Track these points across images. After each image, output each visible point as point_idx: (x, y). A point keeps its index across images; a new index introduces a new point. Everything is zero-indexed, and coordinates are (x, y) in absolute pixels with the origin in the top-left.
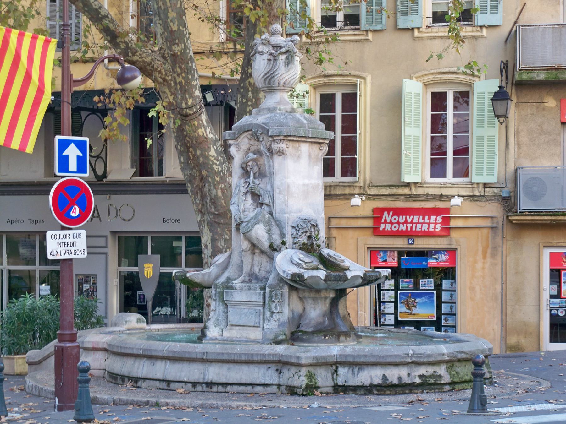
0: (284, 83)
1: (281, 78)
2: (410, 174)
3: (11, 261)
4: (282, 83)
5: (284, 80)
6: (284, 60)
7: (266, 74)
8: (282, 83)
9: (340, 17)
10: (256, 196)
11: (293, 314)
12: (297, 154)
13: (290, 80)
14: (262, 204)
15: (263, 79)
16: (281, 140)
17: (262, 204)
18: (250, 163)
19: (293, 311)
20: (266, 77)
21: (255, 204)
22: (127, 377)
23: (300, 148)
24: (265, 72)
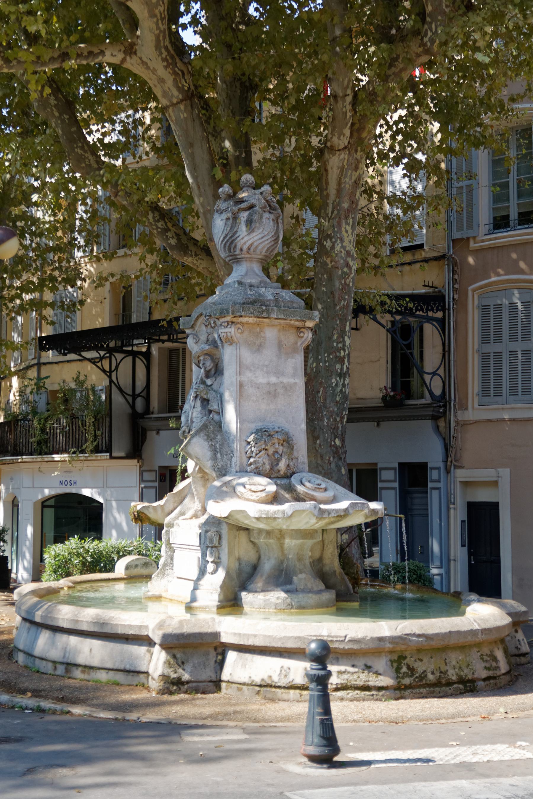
0: (249, 249)
1: (243, 241)
2: (526, 353)
3: (174, 468)
4: (245, 248)
5: (248, 244)
6: (245, 218)
7: (224, 238)
8: (245, 248)
9: (513, 215)
10: (205, 402)
11: (240, 564)
12: (258, 342)
13: (256, 244)
14: (210, 412)
15: (223, 245)
16: (228, 322)
17: (210, 412)
18: (201, 358)
19: (239, 559)
20: (224, 243)
21: (204, 412)
22: (62, 663)
23: (262, 334)
24: (223, 235)
